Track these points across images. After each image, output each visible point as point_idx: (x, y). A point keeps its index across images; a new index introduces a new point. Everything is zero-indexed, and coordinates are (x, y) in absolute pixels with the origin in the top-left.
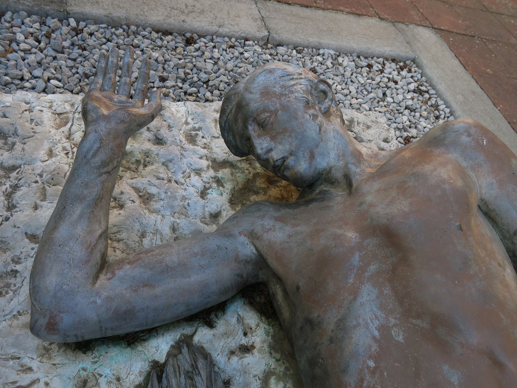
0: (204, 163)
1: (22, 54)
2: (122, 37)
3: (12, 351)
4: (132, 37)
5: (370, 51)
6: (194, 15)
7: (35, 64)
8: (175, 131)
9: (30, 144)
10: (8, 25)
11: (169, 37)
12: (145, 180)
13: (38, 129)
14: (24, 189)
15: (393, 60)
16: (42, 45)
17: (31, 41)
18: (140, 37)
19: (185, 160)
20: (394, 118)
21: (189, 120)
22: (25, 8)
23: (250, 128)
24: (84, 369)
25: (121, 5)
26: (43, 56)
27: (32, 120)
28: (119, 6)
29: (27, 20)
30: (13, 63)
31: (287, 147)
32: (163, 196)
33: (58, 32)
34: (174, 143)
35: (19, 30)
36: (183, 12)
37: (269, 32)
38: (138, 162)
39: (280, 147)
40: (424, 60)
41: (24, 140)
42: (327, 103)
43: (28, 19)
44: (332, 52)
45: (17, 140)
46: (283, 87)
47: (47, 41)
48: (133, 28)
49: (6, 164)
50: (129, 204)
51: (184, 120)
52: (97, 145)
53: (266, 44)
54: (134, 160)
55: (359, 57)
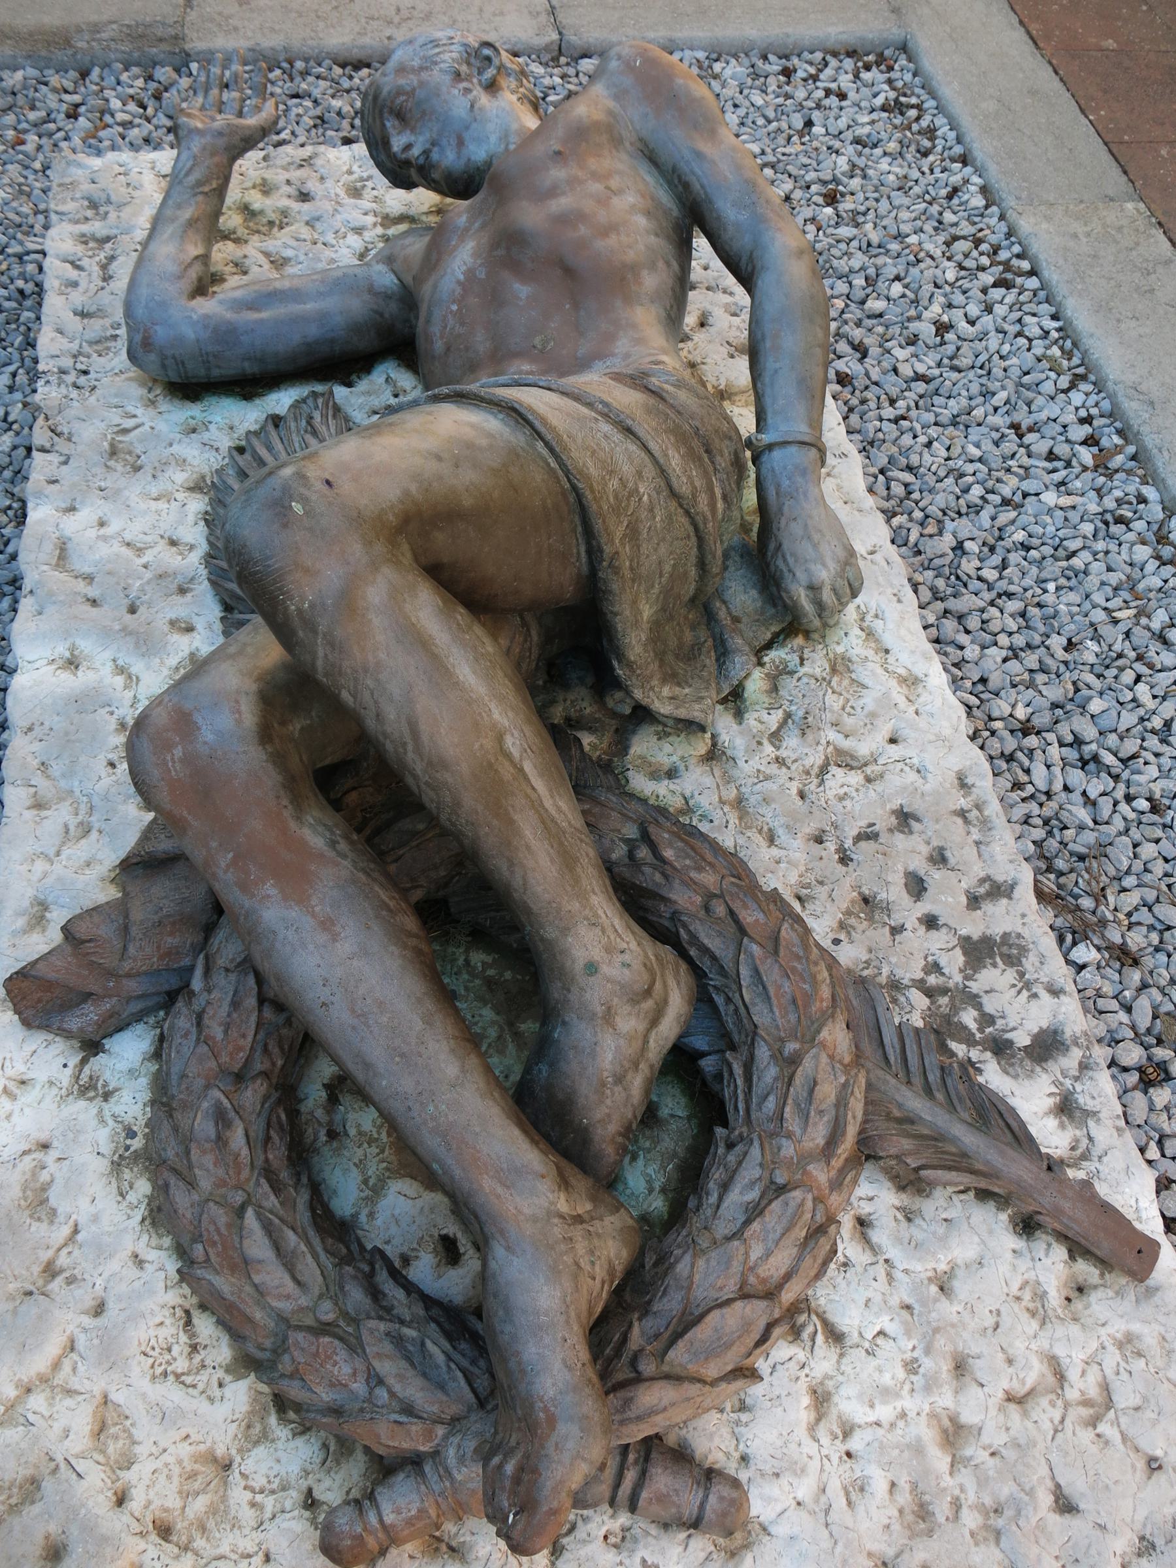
0: (370, 219)
1: (120, 129)
2: (280, 83)
3: (115, 401)
4: (298, 79)
5: (791, 40)
6: (410, 23)
7: (141, 141)
8: (329, 183)
9: (126, 212)
10: (95, 88)
11: (365, 71)
12: (279, 243)
13: (136, 194)
14: (121, 259)
15: (851, 54)
16: (150, 111)
17: (132, 107)
18: (310, 79)
19: (338, 217)
20: (814, 163)
21: (355, 168)
22: (119, 55)
23: (388, 124)
24: (193, 418)
25: (277, 27)
26: (151, 127)
27: (128, 184)
28: (272, 30)
29: (124, 77)
30: (107, 143)
31: (428, 135)
32: (302, 258)
33: (174, 91)
34: (327, 197)
35: (113, 93)
36: (390, 23)
37: (560, 33)
38: (271, 223)
39: (421, 139)
40: (923, 43)
41: (120, 207)
42: (490, 72)
43: (126, 74)
44: (701, 55)
45: (110, 208)
46: (425, 58)
47: (157, 105)
48: (299, 65)
49: (98, 235)
50: (255, 269)
51: (345, 169)
52: (190, 163)
53: (555, 59)
54: (265, 220)
55: (765, 58)
